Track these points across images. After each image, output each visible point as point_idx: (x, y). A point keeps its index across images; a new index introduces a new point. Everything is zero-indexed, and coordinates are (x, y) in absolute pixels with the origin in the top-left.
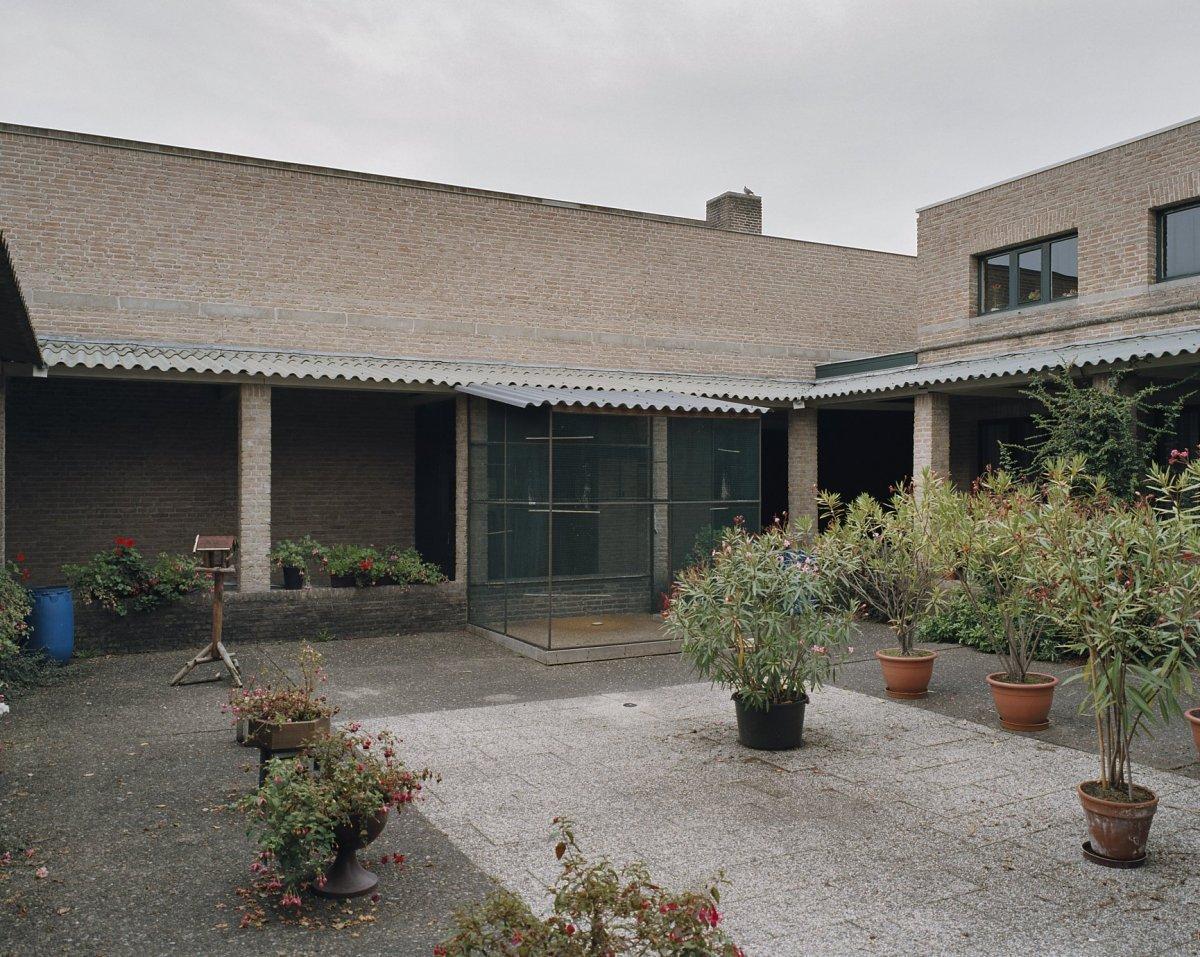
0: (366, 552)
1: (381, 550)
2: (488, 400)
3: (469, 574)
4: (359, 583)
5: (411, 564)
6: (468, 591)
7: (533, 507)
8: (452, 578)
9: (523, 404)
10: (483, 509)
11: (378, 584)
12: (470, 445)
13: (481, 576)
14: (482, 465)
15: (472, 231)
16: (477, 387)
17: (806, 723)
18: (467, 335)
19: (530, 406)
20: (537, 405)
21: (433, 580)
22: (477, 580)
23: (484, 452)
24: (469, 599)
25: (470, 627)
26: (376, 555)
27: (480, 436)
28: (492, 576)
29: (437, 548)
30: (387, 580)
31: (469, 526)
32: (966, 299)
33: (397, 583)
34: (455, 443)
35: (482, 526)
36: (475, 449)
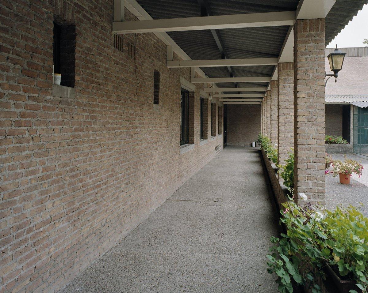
0: (330, 137)
1: (333, 136)
2: (358, 107)
3: (353, 142)
4: (329, 143)
5: (340, 139)
6: (353, 146)
7: (366, 128)
8: (349, 143)
9: (362, 107)
10: (357, 129)
11: (333, 143)
12: (353, 115)
13: (356, 143)
14: (356, 120)
15: (357, 65)
16: (355, 103)
17: (342, 118)
18: (355, 89)
19: (364, 108)
20: (366, 107)
21: (345, 143)
22: (355, 144)
23: (357, 116)
24: (353, 148)
25: (353, 153)
26: (333, 137)
27: (356, 113)
28: (359, 143)
29: (346, 136)
30: (335, 143)
31: (353, 132)
32: (199, 138)
33: (337, 143)
34: (350, 114)
35: (356, 132)
36: (354, 116)
